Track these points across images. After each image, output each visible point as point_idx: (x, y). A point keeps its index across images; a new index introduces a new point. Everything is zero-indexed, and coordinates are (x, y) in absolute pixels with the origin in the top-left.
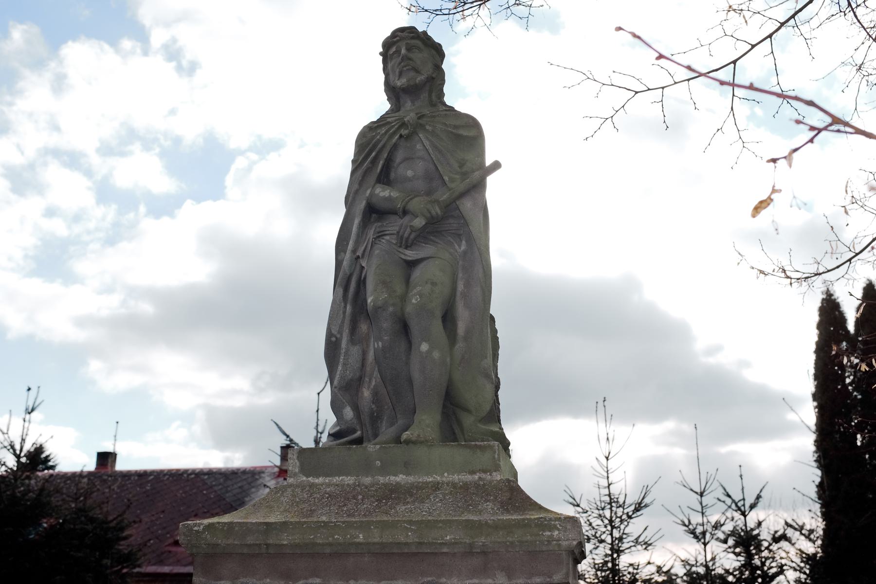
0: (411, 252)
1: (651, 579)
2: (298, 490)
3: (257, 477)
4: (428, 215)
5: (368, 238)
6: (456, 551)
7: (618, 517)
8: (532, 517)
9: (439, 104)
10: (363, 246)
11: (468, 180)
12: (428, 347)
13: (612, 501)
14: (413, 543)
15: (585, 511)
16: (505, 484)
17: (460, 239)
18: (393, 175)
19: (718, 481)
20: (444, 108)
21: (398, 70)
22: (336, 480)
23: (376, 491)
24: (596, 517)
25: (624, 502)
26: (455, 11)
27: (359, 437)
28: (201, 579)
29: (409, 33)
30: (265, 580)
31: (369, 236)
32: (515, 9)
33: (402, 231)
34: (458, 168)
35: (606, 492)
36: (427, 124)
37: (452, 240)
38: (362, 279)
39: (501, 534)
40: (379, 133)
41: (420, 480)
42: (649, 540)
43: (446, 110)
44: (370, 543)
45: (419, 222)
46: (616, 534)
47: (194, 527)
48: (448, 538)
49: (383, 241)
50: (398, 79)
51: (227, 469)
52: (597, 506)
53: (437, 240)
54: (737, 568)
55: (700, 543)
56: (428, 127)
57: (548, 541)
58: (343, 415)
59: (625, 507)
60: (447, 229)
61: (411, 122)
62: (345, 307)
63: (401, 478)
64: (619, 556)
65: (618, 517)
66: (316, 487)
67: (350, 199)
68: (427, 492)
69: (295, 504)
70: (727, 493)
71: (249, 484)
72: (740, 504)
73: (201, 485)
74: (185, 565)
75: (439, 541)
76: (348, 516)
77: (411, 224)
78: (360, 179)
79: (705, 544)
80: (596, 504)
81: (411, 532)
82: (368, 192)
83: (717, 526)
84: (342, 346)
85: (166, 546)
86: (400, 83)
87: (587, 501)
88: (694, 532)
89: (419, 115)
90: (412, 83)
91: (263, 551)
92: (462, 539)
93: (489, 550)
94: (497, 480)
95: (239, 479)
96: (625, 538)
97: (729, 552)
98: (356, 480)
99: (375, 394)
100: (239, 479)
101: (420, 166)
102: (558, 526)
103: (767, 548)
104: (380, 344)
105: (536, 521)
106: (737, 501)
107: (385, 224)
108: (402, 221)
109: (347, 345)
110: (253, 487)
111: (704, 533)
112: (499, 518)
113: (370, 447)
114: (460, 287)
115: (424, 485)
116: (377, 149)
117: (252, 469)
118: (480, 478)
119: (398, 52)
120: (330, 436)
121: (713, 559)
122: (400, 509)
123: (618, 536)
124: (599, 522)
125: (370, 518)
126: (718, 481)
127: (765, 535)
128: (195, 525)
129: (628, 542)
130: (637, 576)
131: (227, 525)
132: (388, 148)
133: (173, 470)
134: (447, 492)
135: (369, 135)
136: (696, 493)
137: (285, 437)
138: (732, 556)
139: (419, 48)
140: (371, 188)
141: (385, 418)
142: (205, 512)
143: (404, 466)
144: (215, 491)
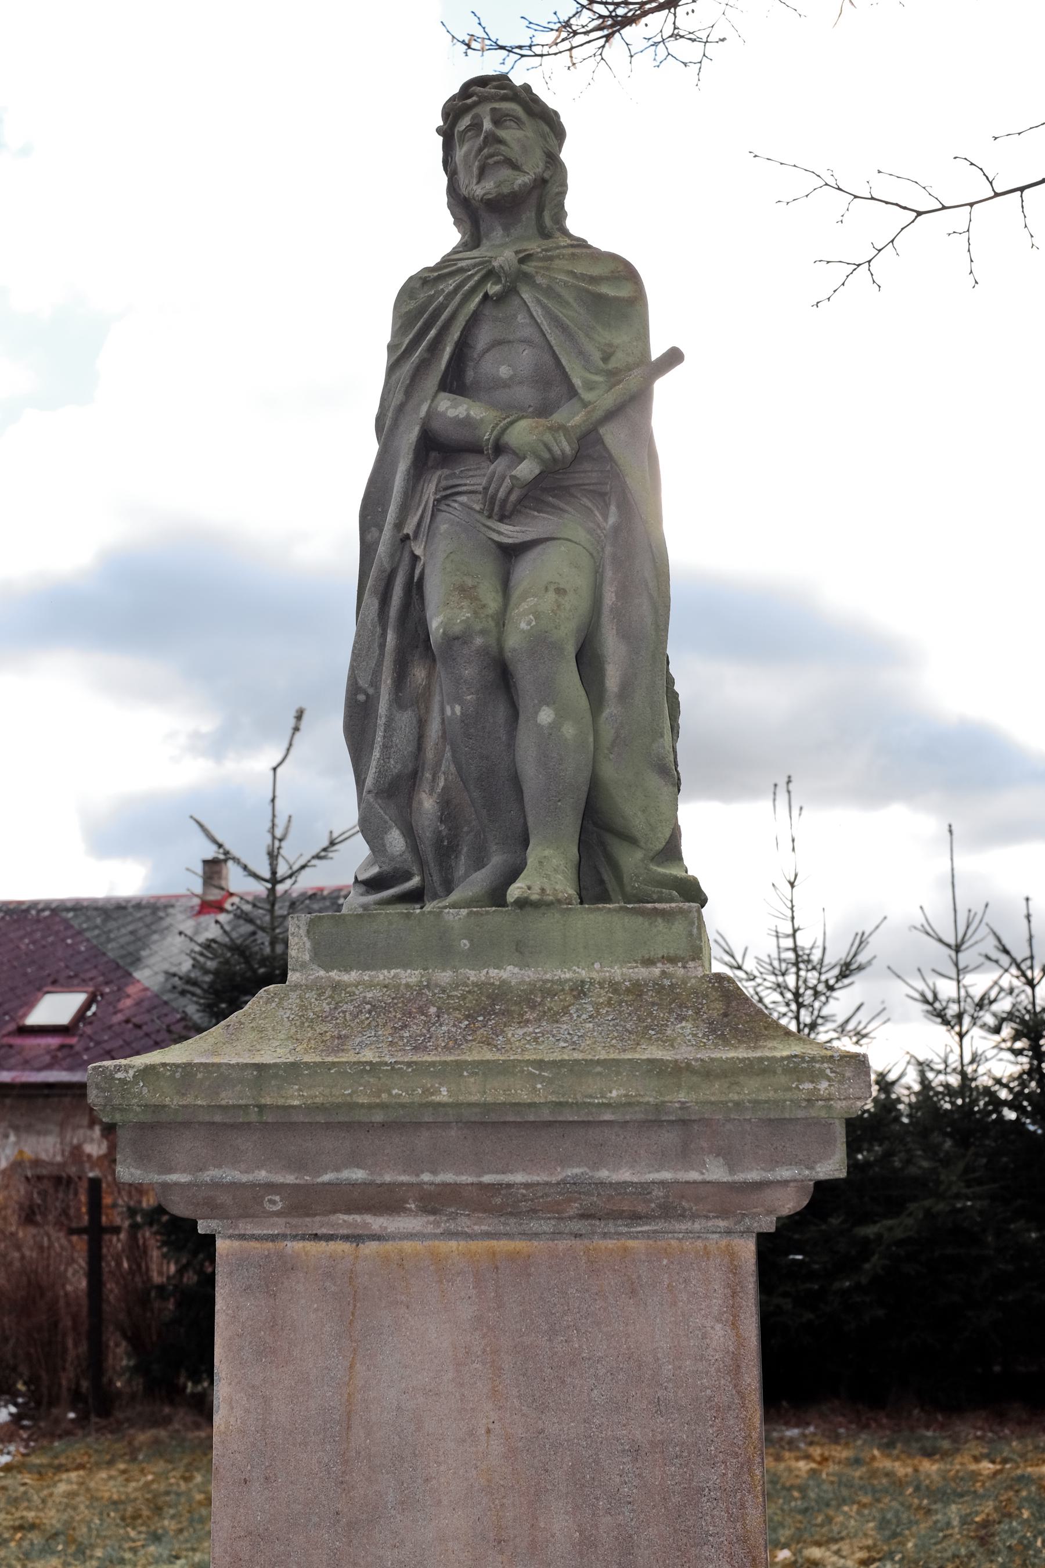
0: (511, 528)
2: (311, 995)
3: (161, 914)
4: (546, 455)
5: (425, 499)
6: (628, 1118)
7: (810, 988)
8: (777, 1054)
9: (558, 234)
10: (415, 514)
11: (621, 386)
12: (553, 716)
13: (800, 959)
14: (545, 1104)
15: (752, 977)
16: (713, 986)
17: (604, 501)
18: (470, 375)
19: (987, 925)
20: (569, 242)
21: (477, 163)
22: (384, 975)
23: (463, 997)
24: (770, 988)
25: (822, 960)
26: (554, 49)
27: (417, 888)
28: (132, 1170)
29: (496, 87)
30: (257, 1171)
31: (426, 496)
32: (673, 45)
33: (493, 485)
34: (601, 363)
35: (789, 943)
36: (537, 273)
37: (589, 504)
38: (415, 580)
39: (717, 1086)
40: (443, 290)
41: (548, 976)
42: (865, 1028)
43: (572, 246)
44: (462, 1104)
45: (527, 470)
46: (806, 1017)
47: (116, 1073)
48: (614, 1094)
49: (456, 505)
50: (478, 182)
51: (108, 900)
52: (774, 968)
53: (562, 505)
54: (1016, 1075)
55: (953, 1033)
56: (539, 280)
57: (808, 1100)
58: (384, 846)
59: (824, 970)
60: (581, 482)
61: (506, 268)
62: (384, 635)
63: (509, 973)
65: (810, 988)
66: (345, 990)
67: (387, 422)
68: (561, 1001)
69: (306, 1024)
70: (1004, 946)
71: (148, 926)
73: (62, 928)
74: (40, 1069)
75: (596, 1101)
76: (416, 1049)
77: (513, 473)
78: (408, 382)
79: (961, 1036)
80: (771, 964)
81: (541, 1083)
83: (982, 1003)
84: (380, 711)
85: (5, 1036)
86: (479, 190)
87: (755, 960)
88: (943, 1013)
89: (521, 255)
90: (506, 190)
91: (253, 1117)
92: (640, 1095)
93: (693, 1117)
94: (696, 977)
96: (822, 1025)
97: (1002, 1049)
98: (422, 976)
99: (446, 804)
100: (129, 919)
101: (525, 358)
102: (828, 1071)
104: (458, 709)
105: (786, 1063)
106: (1019, 959)
107: (457, 472)
108: (492, 467)
109: (389, 709)
110: (155, 932)
111: (959, 1017)
112: (713, 1056)
113: (449, 912)
114: (609, 597)
115: (555, 987)
116: (439, 323)
117: (152, 901)
118: (663, 972)
119: (476, 126)
120: (357, 884)
122: (513, 1035)
123: (808, 1020)
124: (776, 996)
125: (459, 1055)
126: (987, 925)
128: (118, 1068)
129: (826, 1032)
131: (180, 1070)
133: (11, 902)
134: (601, 1001)
135: (422, 296)
136: (948, 946)
137: (214, 848)
138: (1009, 1056)
139: (517, 120)
140: (429, 402)
141: (465, 849)
142: (70, 977)
143: (517, 950)
144: (88, 940)
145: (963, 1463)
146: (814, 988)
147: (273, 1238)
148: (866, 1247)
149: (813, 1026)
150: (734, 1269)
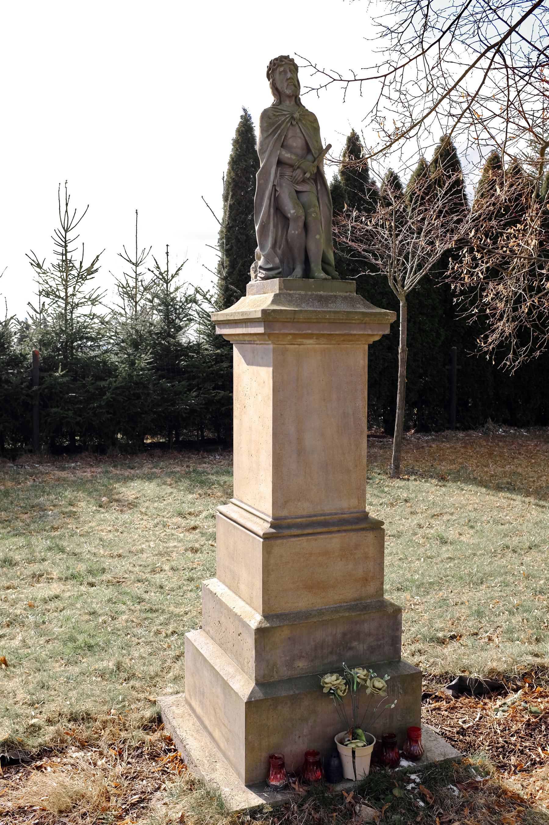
56: (303, 122)
82: (279, 152)
147: (284, 344)
150: (365, 351)
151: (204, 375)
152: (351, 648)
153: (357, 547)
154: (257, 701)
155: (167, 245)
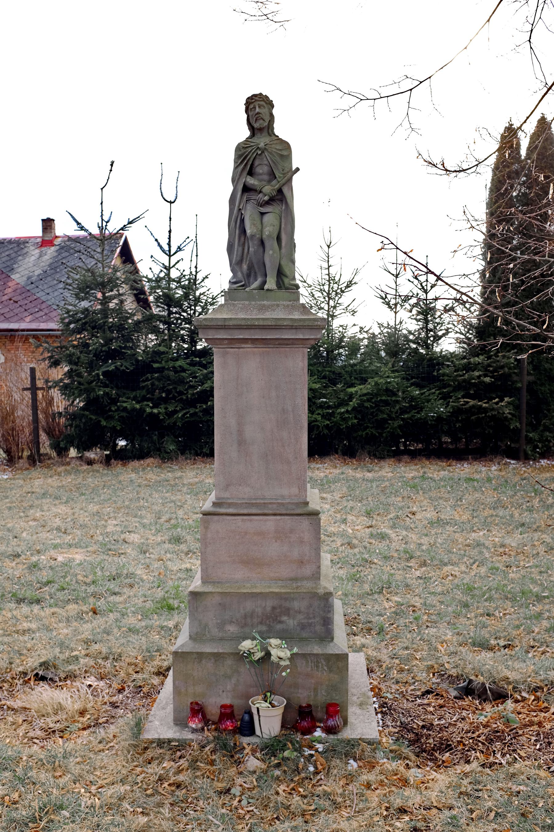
1: (355, 336)
45: (266, 198)
46: (332, 303)
64: (333, 319)
72: (424, 284)
79: (396, 313)
95: (6, 249)
100: (6, 249)
103: (439, 317)
111: (396, 305)
121: (401, 323)
124: (320, 295)
127: (440, 305)
130: (345, 334)
132: (252, 159)
135: (243, 151)
136: (393, 275)
138: (414, 322)
139: (264, 107)
145: (383, 473)
146: (336, 291)
148: (351, 397)
149: (335, 307)
151: (456, 383)
152: (280, 622)
153: (292, 531)
154: (183, 653)
155: (150, 269)
